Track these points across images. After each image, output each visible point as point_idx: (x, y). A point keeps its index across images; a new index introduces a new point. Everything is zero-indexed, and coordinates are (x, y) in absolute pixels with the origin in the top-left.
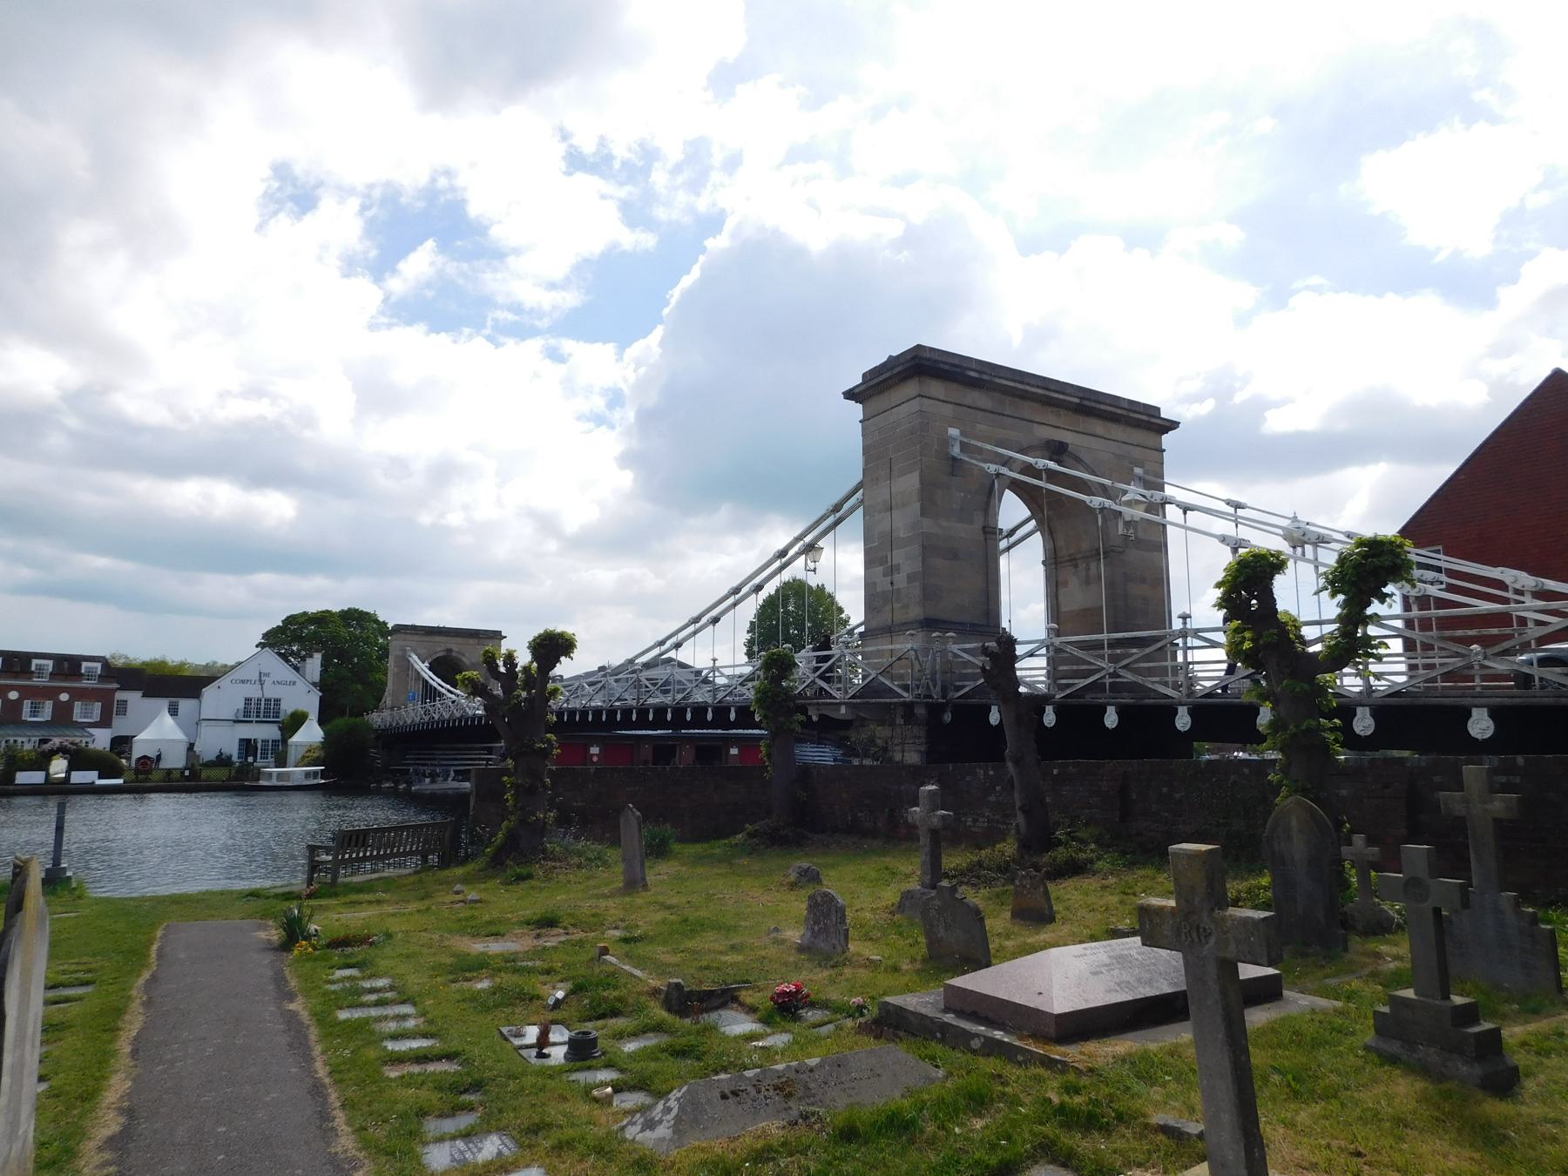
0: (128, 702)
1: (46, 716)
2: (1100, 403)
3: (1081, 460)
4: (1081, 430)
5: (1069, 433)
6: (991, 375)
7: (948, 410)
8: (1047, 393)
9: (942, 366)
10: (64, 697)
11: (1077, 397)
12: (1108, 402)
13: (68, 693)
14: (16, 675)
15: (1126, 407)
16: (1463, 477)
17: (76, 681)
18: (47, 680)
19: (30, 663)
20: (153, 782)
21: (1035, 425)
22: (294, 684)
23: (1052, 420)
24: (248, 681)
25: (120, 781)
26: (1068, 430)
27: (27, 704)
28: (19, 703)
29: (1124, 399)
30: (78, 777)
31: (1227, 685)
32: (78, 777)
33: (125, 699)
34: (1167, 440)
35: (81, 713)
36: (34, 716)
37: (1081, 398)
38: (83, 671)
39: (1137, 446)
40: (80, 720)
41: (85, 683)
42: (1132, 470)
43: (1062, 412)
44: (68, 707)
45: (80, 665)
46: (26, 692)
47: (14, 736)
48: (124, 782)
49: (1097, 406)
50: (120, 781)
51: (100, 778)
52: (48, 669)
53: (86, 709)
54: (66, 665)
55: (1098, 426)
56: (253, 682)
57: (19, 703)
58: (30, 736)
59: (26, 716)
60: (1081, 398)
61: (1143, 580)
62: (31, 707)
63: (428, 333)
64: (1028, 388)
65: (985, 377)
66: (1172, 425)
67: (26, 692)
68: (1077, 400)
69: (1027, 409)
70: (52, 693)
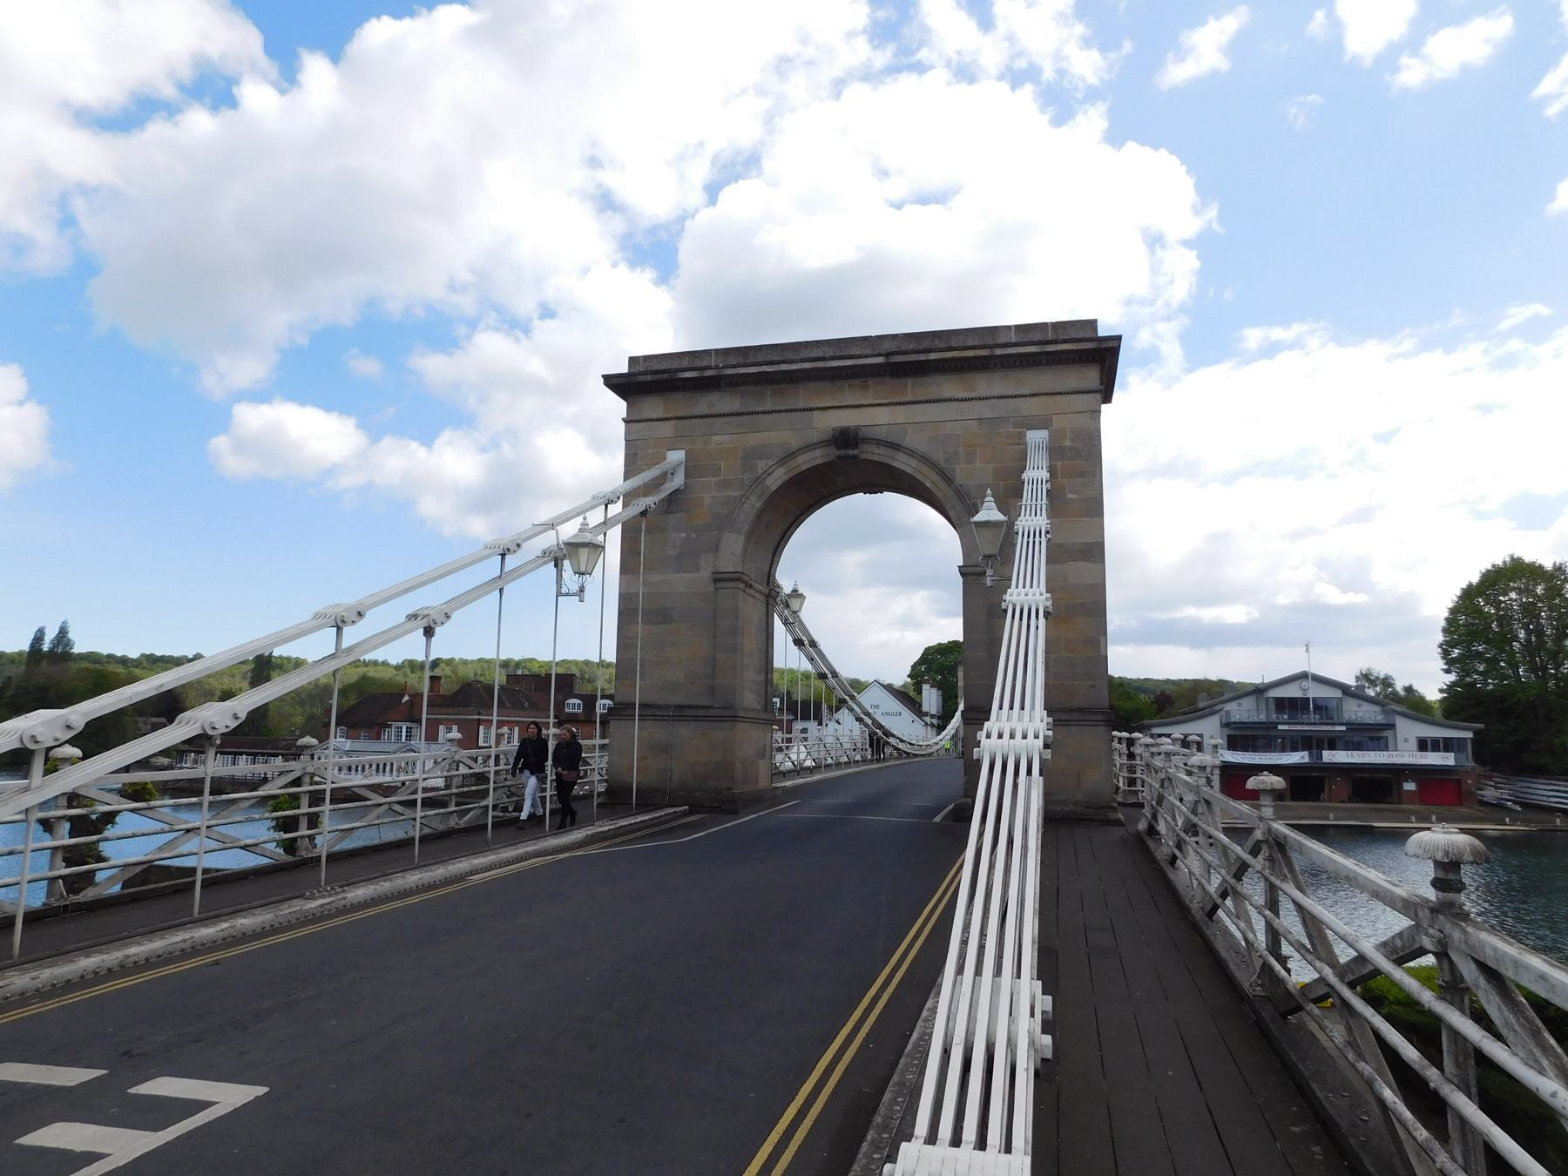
7: (666, 429)
11: (879, 355)
26: (879, 405)
29: (1009, 327)
42: (1022, 436)
55: (948, 386)
68: (880, 360)
69: (803, 397)
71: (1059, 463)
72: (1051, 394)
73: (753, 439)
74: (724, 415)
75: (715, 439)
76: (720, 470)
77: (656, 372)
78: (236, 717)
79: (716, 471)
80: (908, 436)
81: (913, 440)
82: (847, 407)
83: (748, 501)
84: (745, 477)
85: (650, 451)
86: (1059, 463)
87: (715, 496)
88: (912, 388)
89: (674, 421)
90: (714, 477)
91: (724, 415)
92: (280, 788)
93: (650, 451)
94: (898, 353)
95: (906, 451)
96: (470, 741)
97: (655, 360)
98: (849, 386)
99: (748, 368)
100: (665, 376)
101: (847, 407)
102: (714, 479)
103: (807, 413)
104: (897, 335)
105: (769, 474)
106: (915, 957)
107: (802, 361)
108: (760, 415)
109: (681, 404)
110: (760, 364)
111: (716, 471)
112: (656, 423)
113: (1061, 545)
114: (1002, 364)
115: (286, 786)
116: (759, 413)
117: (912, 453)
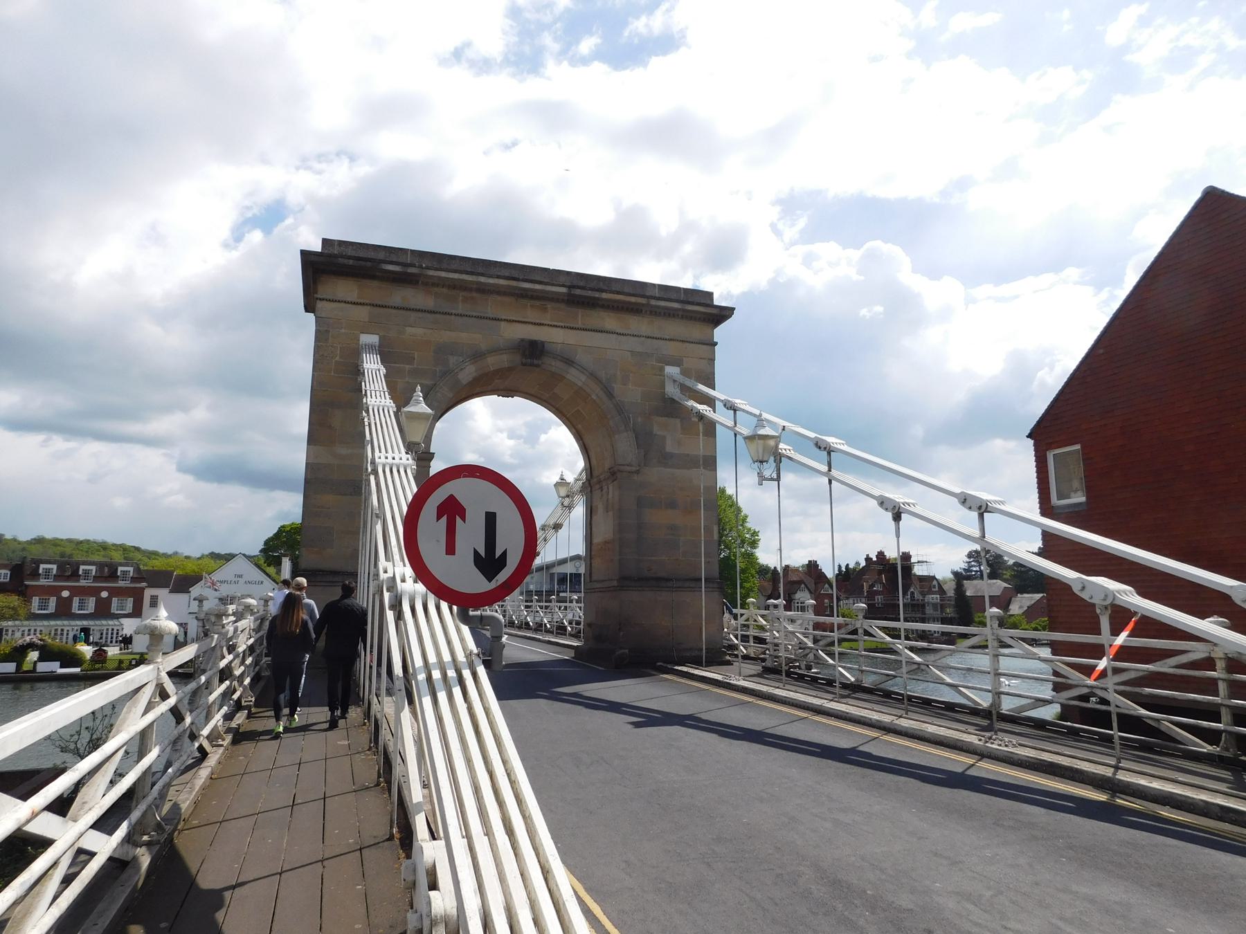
0: (159, 598)
1: (89, 608)
2: (602, 291)
3: (573, 362)
4: (580, 325)
5: (561, 331)
6: (421, 267)
7: (362, 313)
8: (514, 283)
9: (341, 260)
10: (104, 594)
11: (563, 286)
12: (626, 290)
13: (108, 591)
14: (68, 578)
15: (657, 295)
16: (1101, 351)
17: (113, 582)
18: (91, 581)
19: (78, 569)
20: (108, 670)
21: (503, 324)
22: (262, 583)
23: (532, 315)
24: (225, 581)
25: (77, 670)
26: (556, 326)
27: (76, 600)
28: (69, 600)
29: (654, 285)
30: (44, 667)
31: (216, 724)
32: (44, 667)
33: (156, 594)
34: (720, 333)
35: (117, 606)
36: (81, 610)
37: (570, 287)
38: (119, 574)
39: (671, 340)
40: (116, 612)
41: (121, 584)
42: (662, 369)
43: (549, 305)
44: (108, 602)
45: (117, 569)
46: (75, 591)
47: (61, 626)
48: (81, 671)
49: (597, 295)
50: (77, 670)
51: (61, 667)
52: (91, 573)
53: (121, 603)
54: (106, 569)
55: (610, 321)
56: (229, 582)
57: (69, 600)
58: (72, 626)
59: (75, 609)
60: (570, 287)
61: (672, 505)
62: (79, 603)
63: (722, 293)
64: (482, 279)
65: (411, 270)
66: (723, 314)
67: (75, 591)
68: (564, 290)
69: (491, 307)
70: (95, 592)
71: (332, 374)
72: (682, 341)
73: (447, 336)
74: (419, 310)
75: (409, 330)
76: (414, 359)
77: (359, 259)
78: (1091, 598)
79: (410, 359)
80: (578, 356)
81: (582, 358)
82: (529, 323)
83: (441, 390)
84: (438, 369)
85: (343, 331)
86: (332, 374)
87: (408, 382)
88: (583, 317)
89: (369, 307)
90: (407, 364)
91: (419, 310)
92: (1173, 667)
93: (343, 331)
94: (579, 287)
95: (579, 367)
96: (1023, 619)
97: (351, 247)
98: (531, 306)
99: (450, 273)
100: (369, 264)
101: (529, 323)
102: (407, 366)
103: (494, 322)
104: (570, 272)
105: (462, 369)
106: (1225, 770)
107: (498, 277)
108: (453, 317)
109: (374, 291)
110: (461, 272)
111: (410, 359)
112: (350, 305)
113: (688, 455)
114: (651, 312)
115: (1177, 667)
116: (452, 314)
117: (583, 369)
